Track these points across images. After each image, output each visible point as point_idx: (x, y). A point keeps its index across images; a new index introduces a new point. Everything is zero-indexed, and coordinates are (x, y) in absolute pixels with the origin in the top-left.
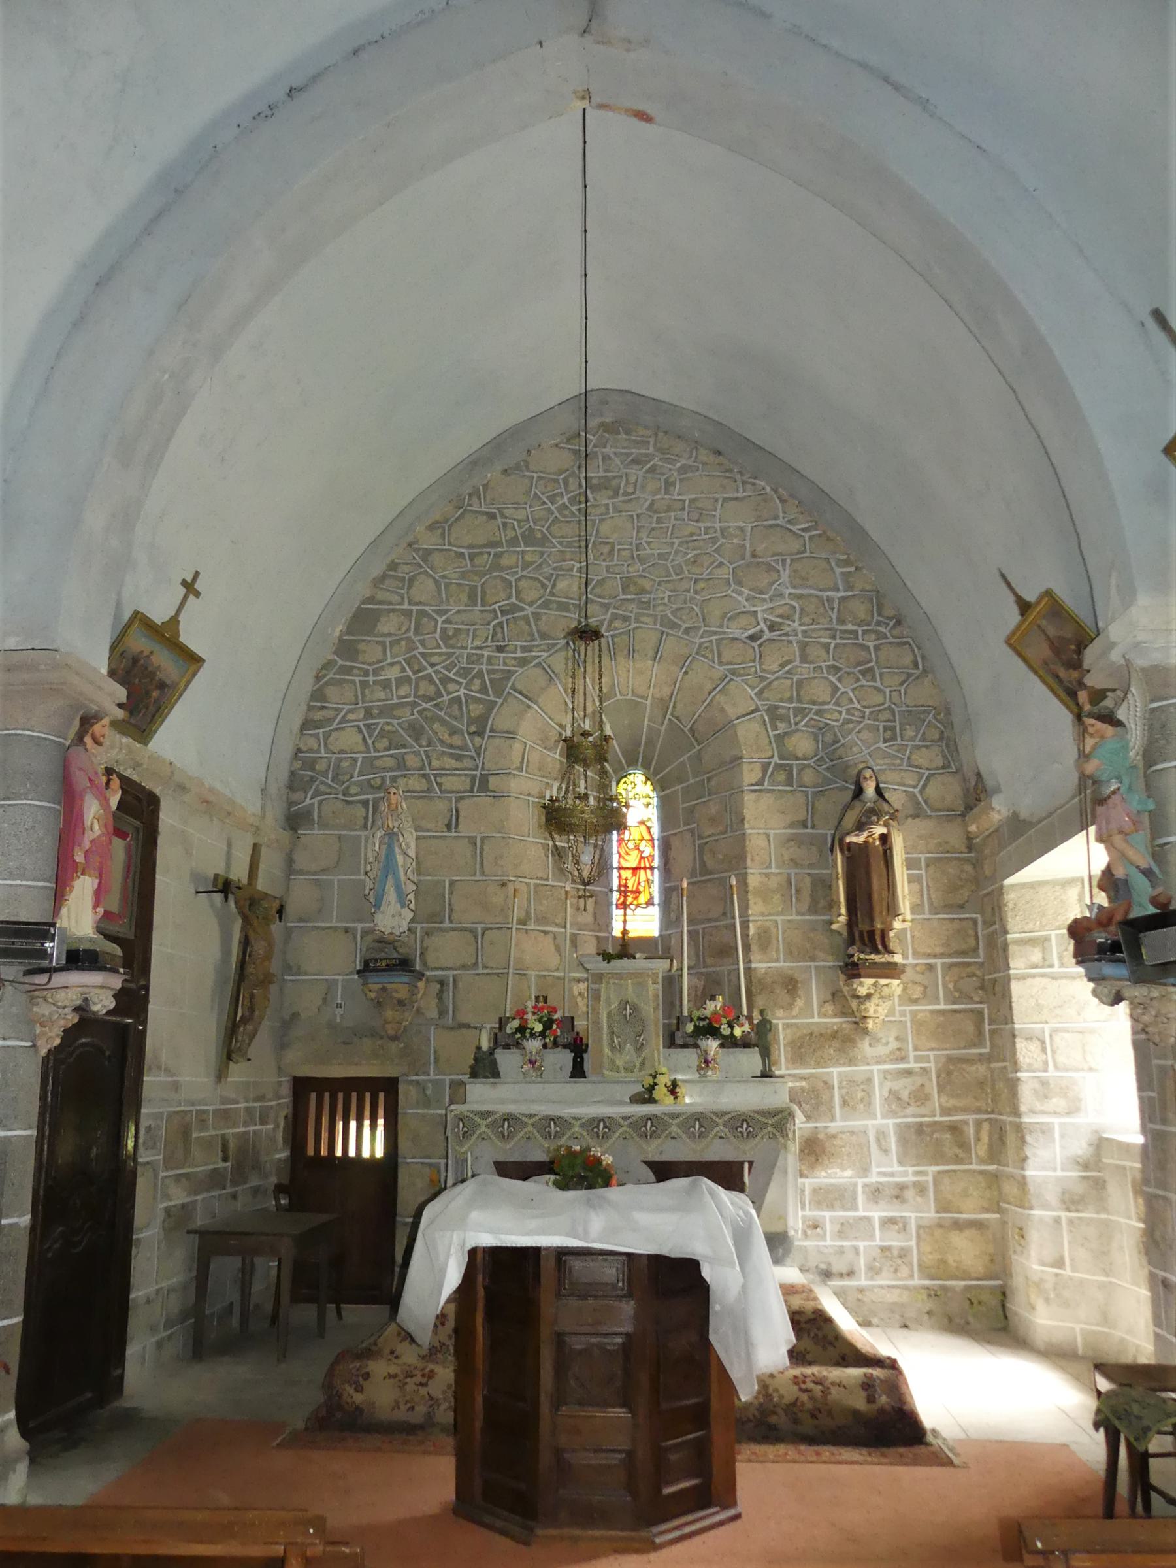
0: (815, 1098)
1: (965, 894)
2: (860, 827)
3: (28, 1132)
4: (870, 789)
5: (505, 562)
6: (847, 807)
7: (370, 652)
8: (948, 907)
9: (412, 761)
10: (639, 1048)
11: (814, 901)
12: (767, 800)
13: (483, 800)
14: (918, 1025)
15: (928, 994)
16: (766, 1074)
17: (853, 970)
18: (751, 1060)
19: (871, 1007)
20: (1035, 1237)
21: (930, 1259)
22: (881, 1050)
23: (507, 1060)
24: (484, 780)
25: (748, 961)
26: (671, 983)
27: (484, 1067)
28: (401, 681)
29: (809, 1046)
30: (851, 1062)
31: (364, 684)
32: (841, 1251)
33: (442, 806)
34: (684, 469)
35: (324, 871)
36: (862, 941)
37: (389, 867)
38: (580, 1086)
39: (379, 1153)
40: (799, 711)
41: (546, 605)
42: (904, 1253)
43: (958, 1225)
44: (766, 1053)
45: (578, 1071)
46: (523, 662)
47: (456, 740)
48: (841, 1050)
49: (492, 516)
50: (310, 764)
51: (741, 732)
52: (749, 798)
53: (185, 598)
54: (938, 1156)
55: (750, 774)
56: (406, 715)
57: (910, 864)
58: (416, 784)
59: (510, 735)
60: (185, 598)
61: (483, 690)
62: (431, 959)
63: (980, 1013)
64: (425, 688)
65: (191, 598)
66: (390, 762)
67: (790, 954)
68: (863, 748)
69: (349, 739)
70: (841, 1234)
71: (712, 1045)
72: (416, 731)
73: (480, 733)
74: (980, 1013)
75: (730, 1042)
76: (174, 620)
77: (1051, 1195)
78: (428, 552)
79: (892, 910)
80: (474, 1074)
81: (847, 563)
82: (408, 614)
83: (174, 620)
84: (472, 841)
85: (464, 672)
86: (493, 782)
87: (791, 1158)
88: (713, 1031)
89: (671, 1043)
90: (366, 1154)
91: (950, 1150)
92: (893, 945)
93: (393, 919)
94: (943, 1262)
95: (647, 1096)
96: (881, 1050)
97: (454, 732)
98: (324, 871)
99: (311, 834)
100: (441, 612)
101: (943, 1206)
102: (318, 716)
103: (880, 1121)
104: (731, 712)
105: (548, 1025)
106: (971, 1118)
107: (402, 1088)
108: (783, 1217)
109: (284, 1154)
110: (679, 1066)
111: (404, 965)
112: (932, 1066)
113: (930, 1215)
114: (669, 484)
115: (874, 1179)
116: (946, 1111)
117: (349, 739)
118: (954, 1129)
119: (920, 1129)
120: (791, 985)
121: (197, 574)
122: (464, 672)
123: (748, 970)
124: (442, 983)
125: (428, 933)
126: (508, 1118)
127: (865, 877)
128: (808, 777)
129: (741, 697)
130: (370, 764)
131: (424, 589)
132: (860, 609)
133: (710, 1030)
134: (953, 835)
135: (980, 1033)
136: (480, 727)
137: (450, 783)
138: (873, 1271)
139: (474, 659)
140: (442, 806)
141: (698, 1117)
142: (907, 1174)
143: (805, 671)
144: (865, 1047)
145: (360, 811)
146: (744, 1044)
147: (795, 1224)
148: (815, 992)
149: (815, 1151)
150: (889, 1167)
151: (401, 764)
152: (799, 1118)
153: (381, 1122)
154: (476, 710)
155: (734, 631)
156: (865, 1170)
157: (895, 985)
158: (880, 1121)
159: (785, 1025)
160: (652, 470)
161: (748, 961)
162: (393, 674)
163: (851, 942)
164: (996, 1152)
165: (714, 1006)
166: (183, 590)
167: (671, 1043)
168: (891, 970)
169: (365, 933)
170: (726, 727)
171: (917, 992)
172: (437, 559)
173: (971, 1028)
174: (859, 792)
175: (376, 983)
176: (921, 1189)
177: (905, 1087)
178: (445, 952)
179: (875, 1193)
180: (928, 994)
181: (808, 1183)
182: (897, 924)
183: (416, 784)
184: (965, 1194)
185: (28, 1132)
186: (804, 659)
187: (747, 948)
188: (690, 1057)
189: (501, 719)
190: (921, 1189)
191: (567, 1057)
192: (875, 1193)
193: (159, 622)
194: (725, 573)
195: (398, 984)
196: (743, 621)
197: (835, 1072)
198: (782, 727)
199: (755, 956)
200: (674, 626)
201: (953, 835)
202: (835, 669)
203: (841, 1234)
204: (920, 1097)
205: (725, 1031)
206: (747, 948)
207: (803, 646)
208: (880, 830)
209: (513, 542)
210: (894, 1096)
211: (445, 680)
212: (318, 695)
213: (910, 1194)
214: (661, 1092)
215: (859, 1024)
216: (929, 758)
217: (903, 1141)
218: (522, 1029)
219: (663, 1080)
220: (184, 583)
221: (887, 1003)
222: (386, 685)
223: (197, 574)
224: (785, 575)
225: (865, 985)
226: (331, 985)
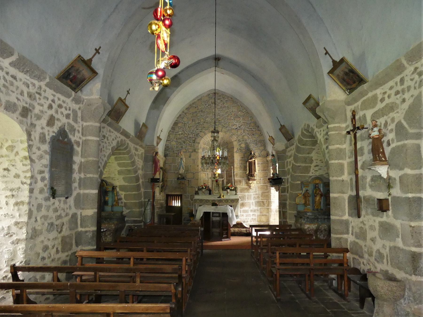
0: (243, 198)
1: (266, 168)
2: (251, 159)
3: (335, 178)
4: (253, 153)
5: (198, 115)
6: (249, 156)
7: (177, 129)
8: (263, 170)
9: (184, 147)
10: (218, 191)
11: (244, 169)
12: (238, 154)
13: (195, 153)
14: (258, 187)
15: (260, 183)
16: (236, 194)
17: (249, 180)
18: (234, 192)
19: (251, 185)
20: (272, 216)
21: (259, 220)
22: (253, 191)
23: (200, 192)
24: (195, 150)
25: (234, 178)
26: (223, 181)
27: (197, 193)
28: (182, 134)
29: (242, 190)
30: (249, 192)
31: (176, 134)
32: (246, 219)
33: (188, 154)
34: (226, 101)
35: (171, 163)
36: (250, 176)
37: (181, 163)
38: (210, 196)
39: (179, 205)
40: (243, 140)
41: (204, 122)
42: (255, 219)
43: (263, 215)
44: (236, 191)
45: (210, 194)
46: (201, 132)
47: (191, 144)
48: (247, 191)
49: (196, 107)
50: (168, 147)
51: (234, 144)
52: (235, 154)
53: (95, 55)
54: (260, 206)
55: (235, 150)
56: (183, 140)
57: (258, 164)
58: (184, 150)
59: (199, 143)
60: (95, 55)
61: (195, 136)
62: (187, 177)
63: (267, 186)
64: (185, 135)
65: (97, 54)
66: (180, 147)
67: (240, 177)
68: (252, 147)
69: (174, 143)
70: (246, 216)
71: (229, 190)
72: (184, 142)
73: (194, 143)
74: (267, 186)
75: (231, 190)
76: (91, 60)
77: (274, 211)
78: (186, 113)
79: (255, 171)
80: (195, 194)
81: (251, 117)
82: (183, 123)
83: (91, 60)
84: (193, 159)
85: (191, 133)
86: (196, 150)
87: (239, 205)
88: (229, 189)
89: (223, 190)
90: (177, 205)
91: (262, 204)
92: (255, 176)
93: (182, 171)
94: (260, 220)
95: (220, 197)
96: (253, 191)
97: (190, 142)
98: (171, 163)
99: (168, 158)
100: (188, 123)
101: (261, 213)
102: (169, 139)
103: (252, 201)
104: (233, 140)
105: (206, 187)
106: (265, 200)
107: (183, 196)
108: (238, 213)
109: (165, 205)
110: (223, 193)
111: (183, 178)
112: (260, 193)
113: (259, 214)
114: (224, 103)
115: (251, 209)
116: (262, 199)
117: (174, 143)
118: (263, 202)
119: (258, 202)
120: (240, 182)
121: (100, 47)
122: (191, 133)
123: (234, 179)
124: (189, 180)
125: (187, 173)
126: (201, 200)
127: (251, 166)
128: (244, 150)
129: (234, 138)
130: (177, 147)
131: (185, 119)
132: (252, 124)
133: (228, 188)
134: (265, 160)
135: (267, 189)
136: (194, 141)
137: (190, 150)
138: (251, 221)
139: (193, 131)
140: (188, 154)
141: (227, 200)
142: (256, 208)
143: (244, 134)
144: (251, 190)
145: (176, 154)
146: (233, 190)
147: (239, 214)
148: (244, 182)
149: (243, 205)
150: (254, 207)
151: (182, 147)
152: (240, 200)
153: (179, 201)
154: (194, 139)
155: (233, 127)
156: (250, 208)
157: (255, 182)
158: (252, 201)
159: (239, 187)
160: (221, 101)
161: (234, 178)
162: (180, 133)
163: (249, 175)
164: (268, 205)
165: (229, 185)
166: (95, 51)
167: (223, 190)
168: (254, 180)
169: (177, 173)
170: (231, 143)
171: (258, 183)
172: (187, 114)
173: (266, 188)
174: (251, 153)
175: (179, 181)
176: (258, 210)
177: (256, 196)
178: (189, 176)
179: (251, 211)
180: (260, 183)
181: (242, 209)
182: (256, 173)
183: (184, 150)
184: (264, 211)
185: (335, 178)
186: (244, 132)
187: (234, 176)
188: (225, 192)
189: (197, 141)
190: (258, 210)
191: (208, 192)
192: (251, 211)
193: (86, 59)
194: (232, 118)
195: (183, 181)
196: (235, 126)
197: (246, 194)
198: (240, 143)
199: (235, 177)
200: (224, 126)
201: (265, 160)
202: (248, 134)
203: (246, 216)
204: (258, 197)
205: (230, 188)
206: (234, 176)
207: (244, 130)
208: (254, 159)
209: (199, 112)
210: (254, 197)
211: (189, 134)
212: (169, 136)
213: (256, 211)
214: (222, 196)
215: (250, 187)
216: (262, 148)
217: (256, 204)
218: (202, 188)
219: (222, 195)
220: (96, 49)
221: (254, 184)
222: (179, 134)
223: (100, 47)
224: (241, 119)
225: (251, 182)
226: (172, 181)
